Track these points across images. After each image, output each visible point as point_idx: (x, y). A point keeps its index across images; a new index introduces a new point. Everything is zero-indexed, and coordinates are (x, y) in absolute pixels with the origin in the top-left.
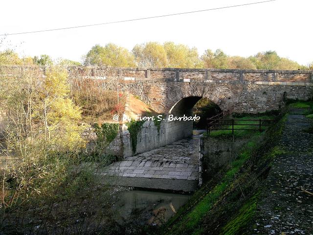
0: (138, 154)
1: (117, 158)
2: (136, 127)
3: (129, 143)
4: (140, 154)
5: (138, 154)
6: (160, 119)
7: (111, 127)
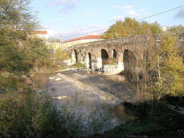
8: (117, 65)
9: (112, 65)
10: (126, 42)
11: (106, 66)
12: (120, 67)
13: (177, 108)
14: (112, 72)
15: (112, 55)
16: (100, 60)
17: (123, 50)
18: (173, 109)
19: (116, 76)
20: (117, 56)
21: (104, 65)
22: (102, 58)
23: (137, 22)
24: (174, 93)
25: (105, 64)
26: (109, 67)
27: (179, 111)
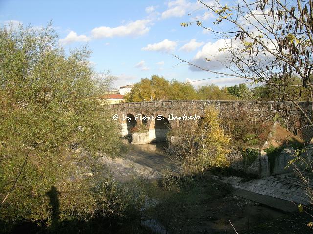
0: (276, 175)
1: (255, 177)
2: (274, 155)
3: (268, 166)
4: (278, 174)
5: (276, 175)
6: (160, 119)
7: (252, 152)
9: (142, 133)
11: (135, 135)
12: (152, 135)
13: (220, 178)
18: (216, 179)
19: (146, 146)
23: (166, 82)
24: (219, 165)
27: (222, 181)
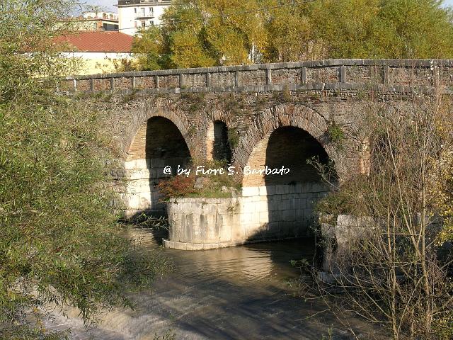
8: (234, 200)
9: (212, 202)
10: (285, 87)
14: (211, 234)
15: (210, 148)
16: (137, 168)
17: (269, 125)
19: (228, 257)
20: (237, 154)
21: (172, 200)
22: (146, 158)
25: (178, 196)
26: (197, 212)
